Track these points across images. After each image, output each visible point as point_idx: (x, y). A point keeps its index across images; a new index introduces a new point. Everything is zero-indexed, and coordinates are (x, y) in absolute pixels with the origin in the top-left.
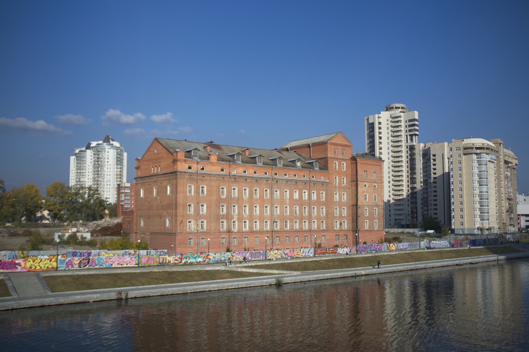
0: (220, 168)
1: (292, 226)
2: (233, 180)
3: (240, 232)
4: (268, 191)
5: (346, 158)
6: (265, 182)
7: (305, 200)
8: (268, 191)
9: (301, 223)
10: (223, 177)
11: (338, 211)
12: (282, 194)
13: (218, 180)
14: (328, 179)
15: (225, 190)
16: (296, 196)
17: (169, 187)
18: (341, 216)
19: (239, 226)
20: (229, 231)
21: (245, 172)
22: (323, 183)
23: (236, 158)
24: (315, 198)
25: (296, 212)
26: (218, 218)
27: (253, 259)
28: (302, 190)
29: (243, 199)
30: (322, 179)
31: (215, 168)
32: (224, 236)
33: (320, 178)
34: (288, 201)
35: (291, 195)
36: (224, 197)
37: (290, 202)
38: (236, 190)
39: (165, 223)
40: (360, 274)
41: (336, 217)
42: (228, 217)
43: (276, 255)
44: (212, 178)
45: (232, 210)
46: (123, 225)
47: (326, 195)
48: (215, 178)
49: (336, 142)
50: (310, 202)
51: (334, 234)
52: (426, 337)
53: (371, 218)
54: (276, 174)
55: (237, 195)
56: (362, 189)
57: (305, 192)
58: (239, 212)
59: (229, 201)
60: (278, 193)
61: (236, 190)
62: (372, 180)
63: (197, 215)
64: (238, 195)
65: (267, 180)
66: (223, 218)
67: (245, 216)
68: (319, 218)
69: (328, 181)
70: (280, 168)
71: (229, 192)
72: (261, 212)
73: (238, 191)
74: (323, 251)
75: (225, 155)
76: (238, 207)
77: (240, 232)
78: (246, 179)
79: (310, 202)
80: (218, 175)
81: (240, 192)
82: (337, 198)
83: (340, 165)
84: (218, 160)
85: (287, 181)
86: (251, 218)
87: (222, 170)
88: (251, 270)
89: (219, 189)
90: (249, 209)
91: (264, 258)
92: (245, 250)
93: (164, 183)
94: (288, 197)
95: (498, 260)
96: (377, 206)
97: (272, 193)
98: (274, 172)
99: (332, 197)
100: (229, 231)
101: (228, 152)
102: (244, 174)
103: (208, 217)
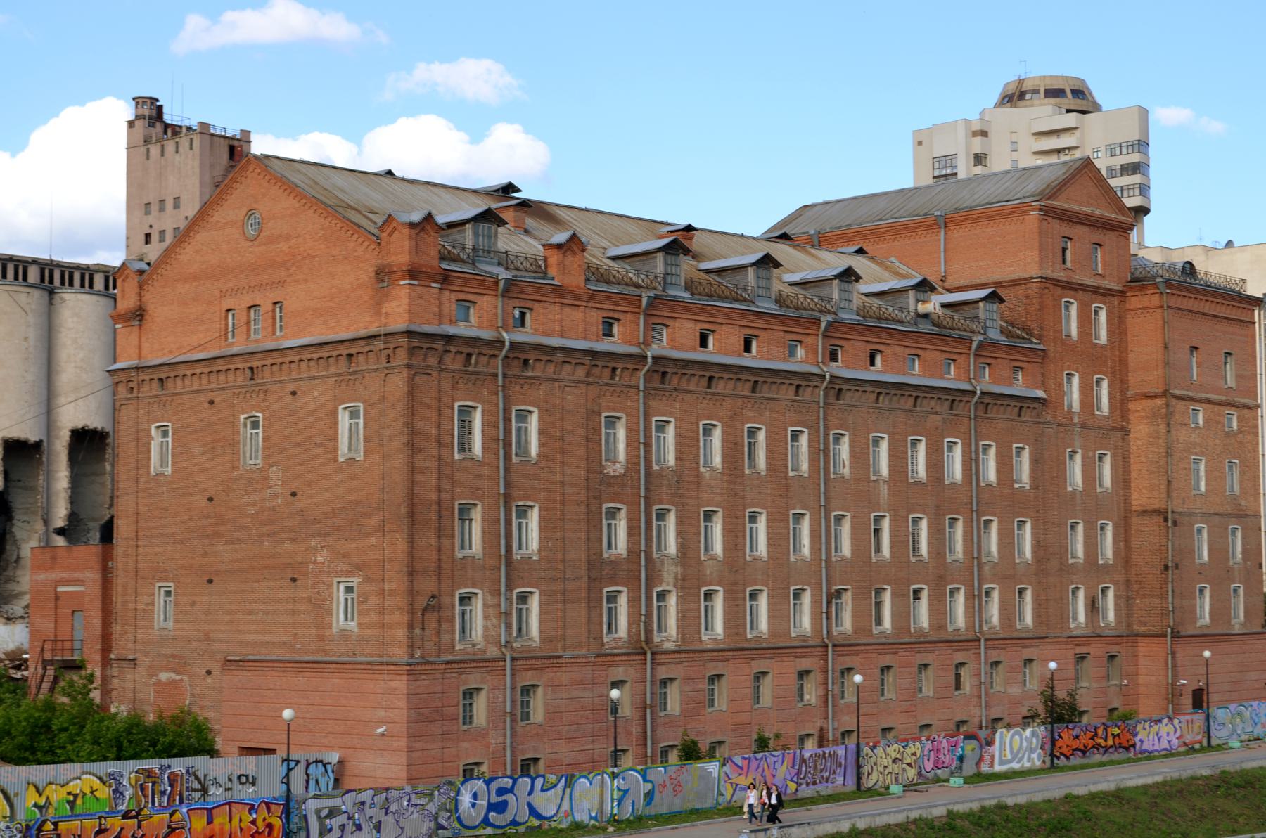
1: (902, 616)
3: (691, 650)
9: (977, 600)
12: (862, 456)
18: (509, 504)
19: (682, 618)
20: (643, 649)
25: (916, 543)
27: (806, 791)
30: (1019, 387)
32: (619, 673)
34: (884, 489)
35: (899, 459)
39: (322, 609)
40: (855, 755)
42: (640, 571)
43: (896, 768)
47: (1035, 461)
48: (580, 373)
49: (1071, 206)
52: (18, 668)
55: (671, 460)
58: (682, 547)
64: (679, 458)
66: (613, 580)
67: (709, 570)
71: (642, 444)
72: (735, 540)
73: (679, 438)
74: (1085, 740)
76: (679, 521)
78: (711, 373)
80: (595, 354)
81: (688, 447)
82: (1076, 474)
83: (1087, 321)
90: (726, 532)
91: (851, 786)
92: (762, 744)
94: (885, 471)
100: (643, 649)
101: (605, 243)
102: (700, 356)
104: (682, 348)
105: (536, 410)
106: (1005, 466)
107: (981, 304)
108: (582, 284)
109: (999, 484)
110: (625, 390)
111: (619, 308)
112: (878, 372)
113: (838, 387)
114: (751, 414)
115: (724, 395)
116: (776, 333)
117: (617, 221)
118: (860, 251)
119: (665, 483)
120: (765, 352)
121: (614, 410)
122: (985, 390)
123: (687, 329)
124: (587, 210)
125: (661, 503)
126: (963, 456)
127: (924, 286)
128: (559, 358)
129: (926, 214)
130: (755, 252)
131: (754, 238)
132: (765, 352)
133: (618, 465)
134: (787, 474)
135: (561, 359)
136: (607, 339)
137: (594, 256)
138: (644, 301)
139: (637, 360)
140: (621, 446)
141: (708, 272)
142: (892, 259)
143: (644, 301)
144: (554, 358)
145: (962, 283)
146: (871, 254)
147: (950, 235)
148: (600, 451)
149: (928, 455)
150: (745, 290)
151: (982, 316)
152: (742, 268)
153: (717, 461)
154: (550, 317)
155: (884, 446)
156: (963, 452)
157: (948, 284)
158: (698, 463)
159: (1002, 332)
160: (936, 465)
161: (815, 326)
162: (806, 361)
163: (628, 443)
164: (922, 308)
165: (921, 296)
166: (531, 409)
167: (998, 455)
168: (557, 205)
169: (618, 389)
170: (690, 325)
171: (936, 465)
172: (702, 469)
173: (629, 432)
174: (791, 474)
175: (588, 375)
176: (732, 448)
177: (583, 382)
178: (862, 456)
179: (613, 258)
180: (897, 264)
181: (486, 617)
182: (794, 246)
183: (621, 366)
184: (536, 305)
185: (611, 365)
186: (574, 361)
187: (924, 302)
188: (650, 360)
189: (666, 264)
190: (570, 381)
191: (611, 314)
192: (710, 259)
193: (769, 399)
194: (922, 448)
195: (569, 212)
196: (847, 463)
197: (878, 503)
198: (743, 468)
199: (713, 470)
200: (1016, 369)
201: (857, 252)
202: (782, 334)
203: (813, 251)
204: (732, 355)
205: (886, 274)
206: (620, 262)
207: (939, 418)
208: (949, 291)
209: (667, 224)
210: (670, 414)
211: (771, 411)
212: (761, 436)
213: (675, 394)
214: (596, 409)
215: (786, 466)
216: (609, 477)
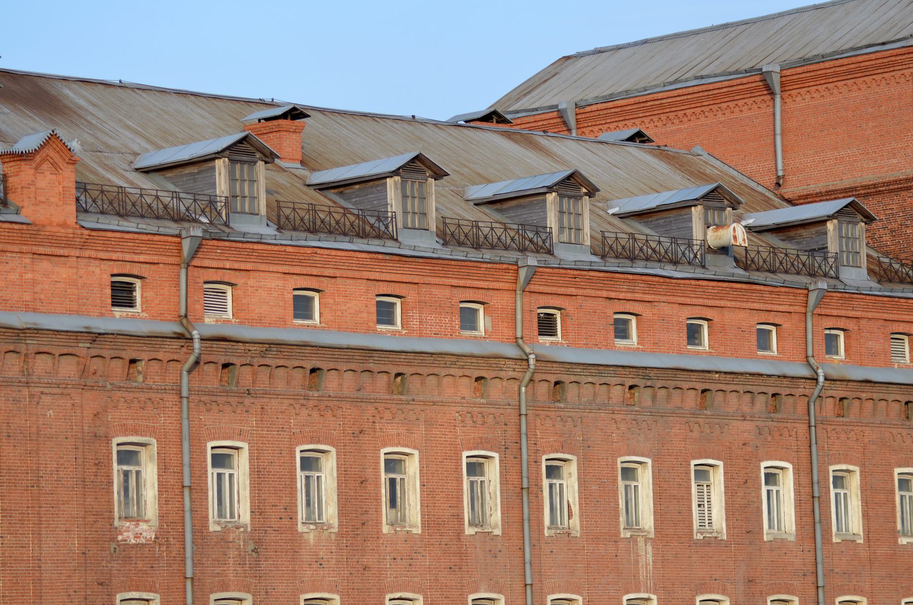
0: (100, 277)
2: (211, 376)
4: (493, 471)
6: (465, 388)
7: (779, 544)
8: (493, 471)
10: (129, 350)
12: (599, 496)
13: (86, 382)
15: (150, 471)
16: (713, 510)
21: (302, 307)
23: (222, 186)
24: (855, 523)
28: (753, 460)
29: (295, 540)
31: (63, 272)
34: (647, 554)
36: (147, 531)
37: (661, 560)
38: (242, 466)
44: (42, 364)
45: (300, 484)
48: (68, 369)
54: (546, 326)
55: (244, 513)
57: (771, 478)
60: (570, 482)
61: (242, 466)
64: (257, 510)
65: (481, 370)
70: (577, 272)
71: (183, 488)
73: (258, 475)
75: (117, 161)
78: (314, 364)
80: (95, 337)
84: (82, 210)
85: (638, 378)
87: (122, 295)
89: (103, 465)
94: (647, 519)
95: (570, 229)
97: (521, 493)
98: (537, 305)
101: (137, 144)
102: (296, 331)
104: (259, 321)
105: (416, 453)
106: (812, 505)
107: (551, 197)
108: (72, 220)
109: (868, 538)
110: (155, 396)
111: (142, 258)
112: (630, 350)
113: (558, 381)
114: (392, 430)
115: (340, 399)
116: (435, 291)
117: (177, 103)
118: (638, 137)
119: (232, 553)
120: (415, 324)
121: (136, 432)
122: (834, 374)
123: (270, 290)
124: (122, 86)
125: (225, 588)
126: (797, 492)
127: (719, 199)
128: (33, 344)
129: (752, 69)
130: (410, 151)
131: (436, 124)
132: (415, 324)
133: (143, 526)
134: (460, 532)
135: (33, 349)
136: (118, 312)
137: (112, 170)
138: (186, 245)
139: (176, 344)
140: (150, 493)
141: (323, 188)
142: (698, 149)
143: (186, 245)
144: (22, 348)
145: (814, 188)
146: (658, 141)
147: (790, 104)
148: (110, 502)
149: (729, 491)
150: (690, 246)
151: (833, 246)
152: (380, 179)
153: (330, 512)
154: (14, 277)
155: (645, 479)
156: (798, 484)
157: (789, 191)
158: (293, 518)
159: (870, 271)
160: (744, 509)
161: (509, 277)
162: (488, 335)
163: (163, 487)
164: (715, 238)
165: (713, 216)
166: (851, 467)
167: (865, 488)
168: (65, 79)
169: (142, 396)
170: (273, 282)
171: (744, 509)
172: (301, 528)
173: (163, 469)
174: (469, 531)
175: (84, 372)
176: (354, 487)
177: (75, 387)
178: (599, 496)
179: (147, 171)
180: (706, 157)
182: (508, 135)
183: (145, 356)
184: (324, 284)
185: (129, 354)
186: (57, 352)
187: (719, 226)
188: (197, 345)
189: (232, 179)
190: (50, 385)
191: (127, 269)
192: (336, 165)
193: (425, 403)
194: (718, 479)
195: (85, 91)
196: (576, 509)
197: (636, 576)
198: (378, 523)
199: (321, 527)
200: (895, 337)
201: (631, 139)
202: (447, 292)
203: (544, 141)
204: (354, 330)
205: (676, 177)
206: (156, 176)
207: (748, 425)
208: (791, 202)
209: (262, 103)
210: (240, 436)
211: (429, 423)
212: (413, 467)
213: (248, 401)
214: (101, 431)
215: (459, 518)
216: (126, 547)
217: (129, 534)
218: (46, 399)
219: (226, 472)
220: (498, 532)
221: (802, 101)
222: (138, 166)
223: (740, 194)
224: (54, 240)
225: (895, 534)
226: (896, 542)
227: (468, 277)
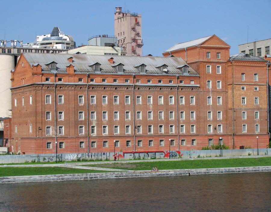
5: (221, 61)
11: (212, 115)
12: (145, 101)
14: (200, 84)
16: (162, 101)
17: (31, 98)
22: (192, 88)
26: (77, 124)
29: (102, 105)
33: (190, 83)
34: (151, 106)
41: (209, 120)
42: (88, 122)
46: (5, 133)
48: (73, 88)
49: (208, 46)
50: (179, 109)
51: (207, 138)
53: (251, 121)
56: (238, 92)
59: (89, 109)
62: (253, 82)
63: (56, 121)
64: (97, 102)
68: (187, 122)
69: (198, 85)
77: (99, 137)
79: (179, 109)
85: (150, 87)
86: (111, 122)
88: (95, 168)
93: (28, 93)
96: (259, 109)
99: (204, 101)
103: (67, 123)
119: (94, 107)
179: (178, 68)
181: (52, 130)
197: (150, 109)
210: (95, 94)
211: (120, 93)
216: (80, 106)
217: (80, 105)
218: (70, 91)
219: (182, 99)
220: (163, 104)
221: (189, 52)
222: (177, 67)
223: (47, 63)
224: (71, 75)
225: (190, 104)
226: (190, 105)
227: (126, 76)
